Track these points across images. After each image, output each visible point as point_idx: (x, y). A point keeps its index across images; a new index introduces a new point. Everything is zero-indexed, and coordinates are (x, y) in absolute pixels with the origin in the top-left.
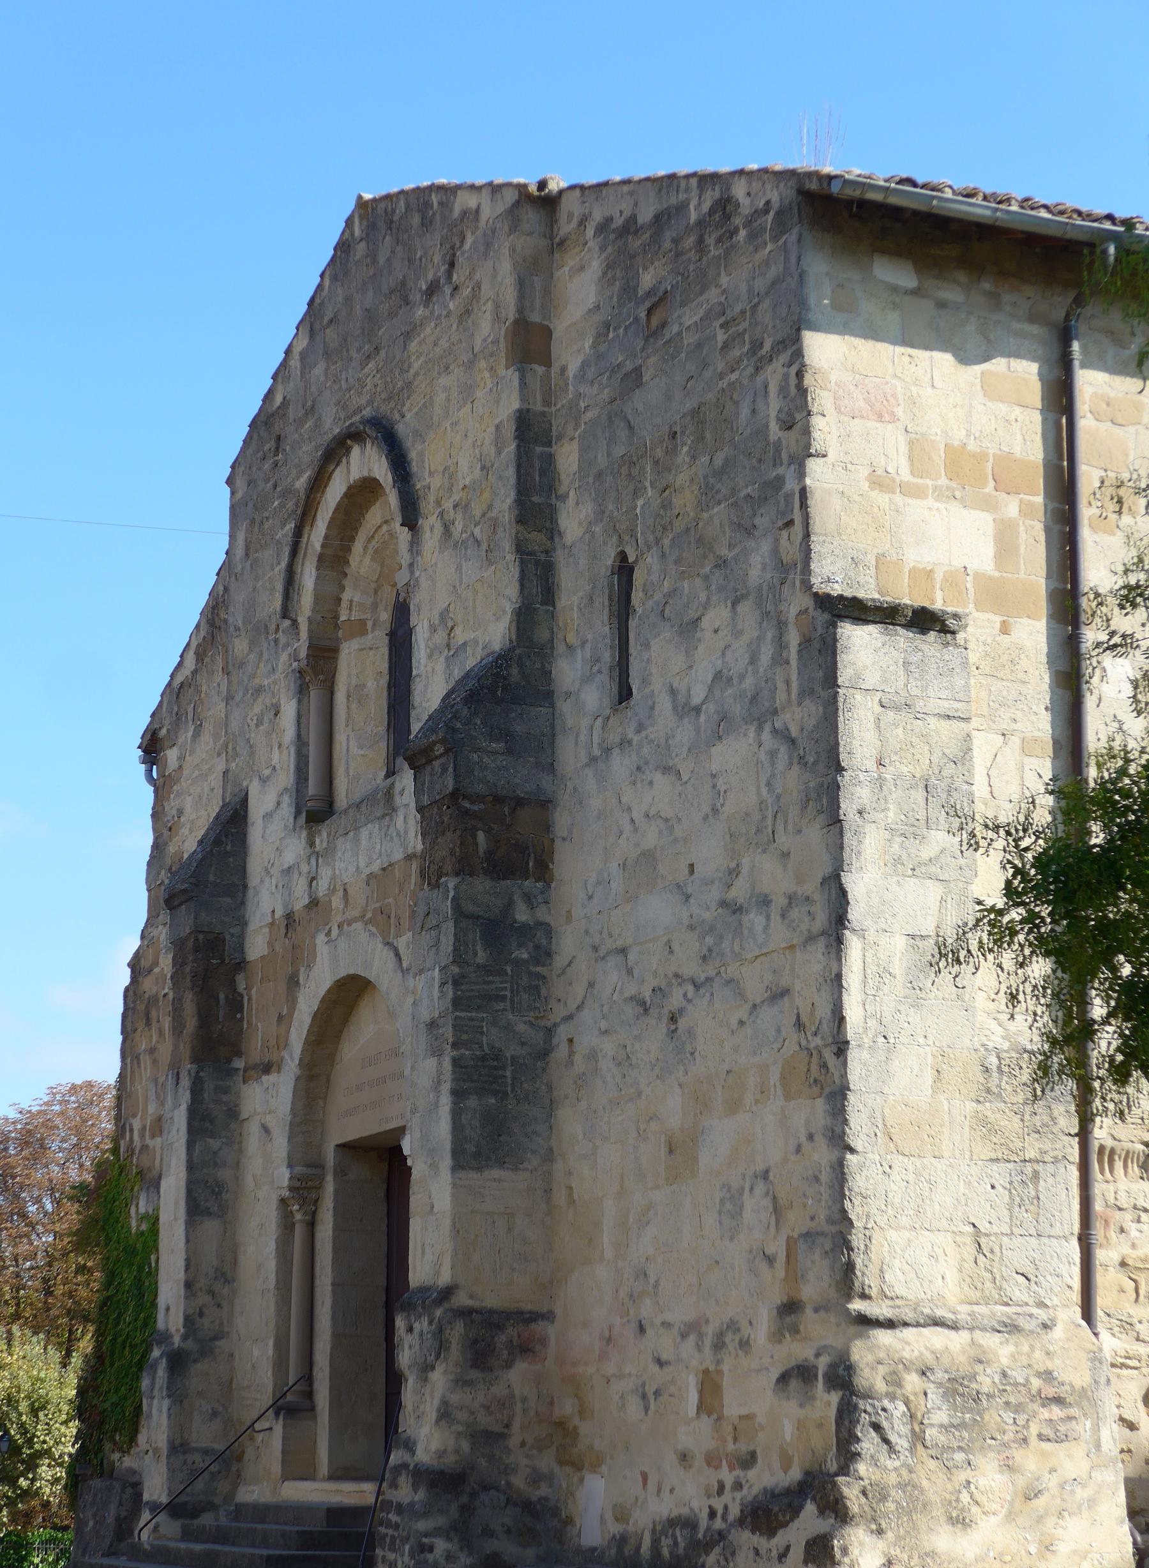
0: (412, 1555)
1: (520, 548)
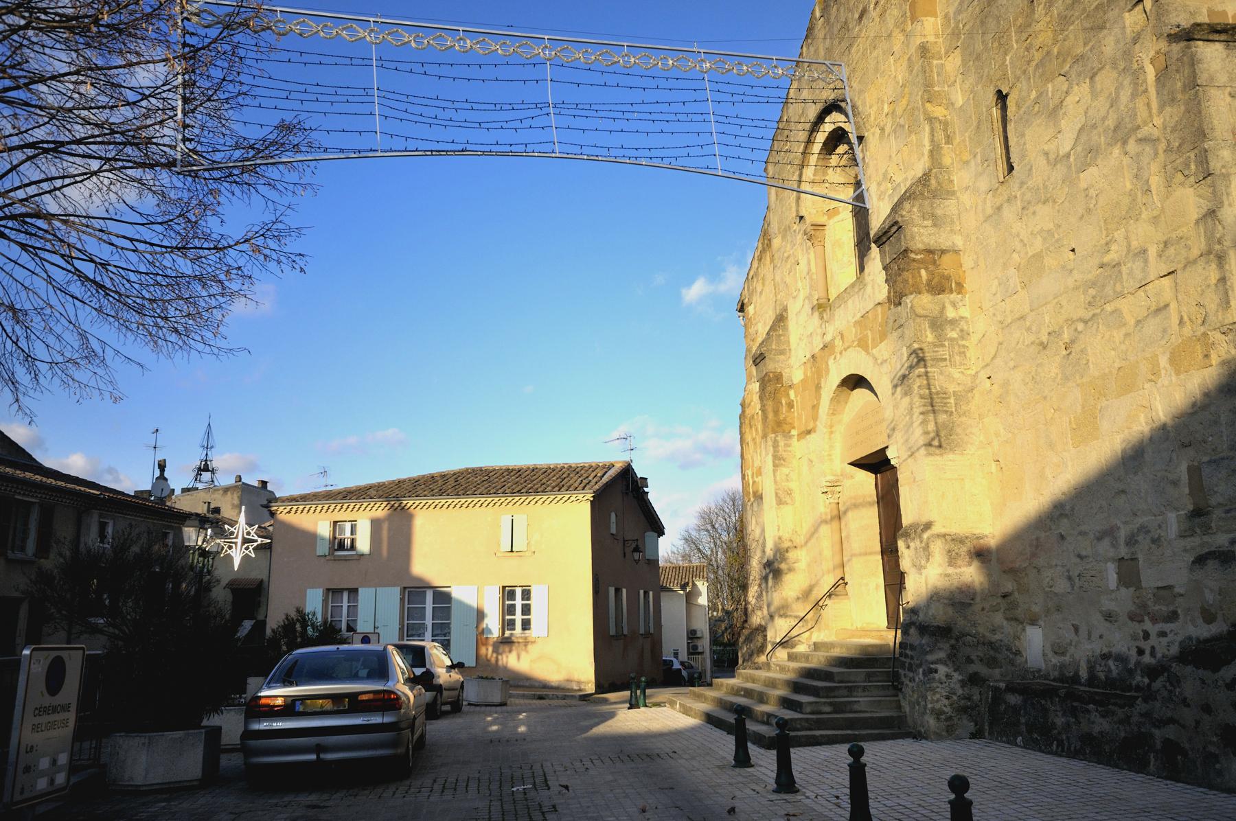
0: (924, 674)
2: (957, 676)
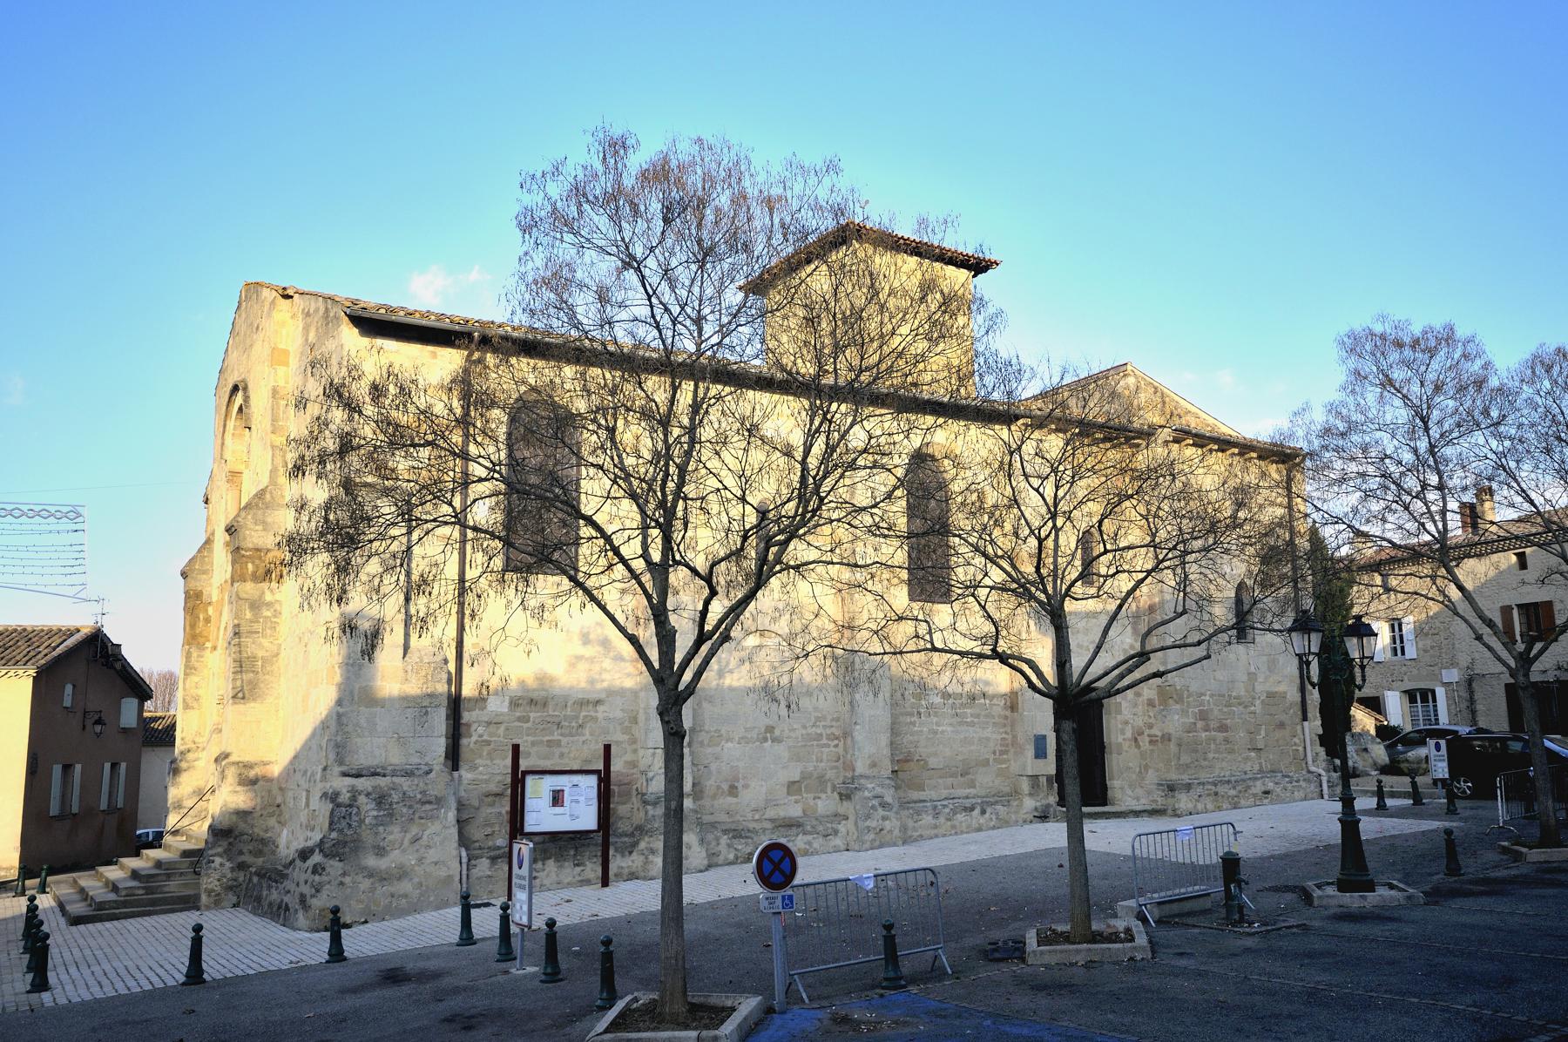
2: (228, 865)
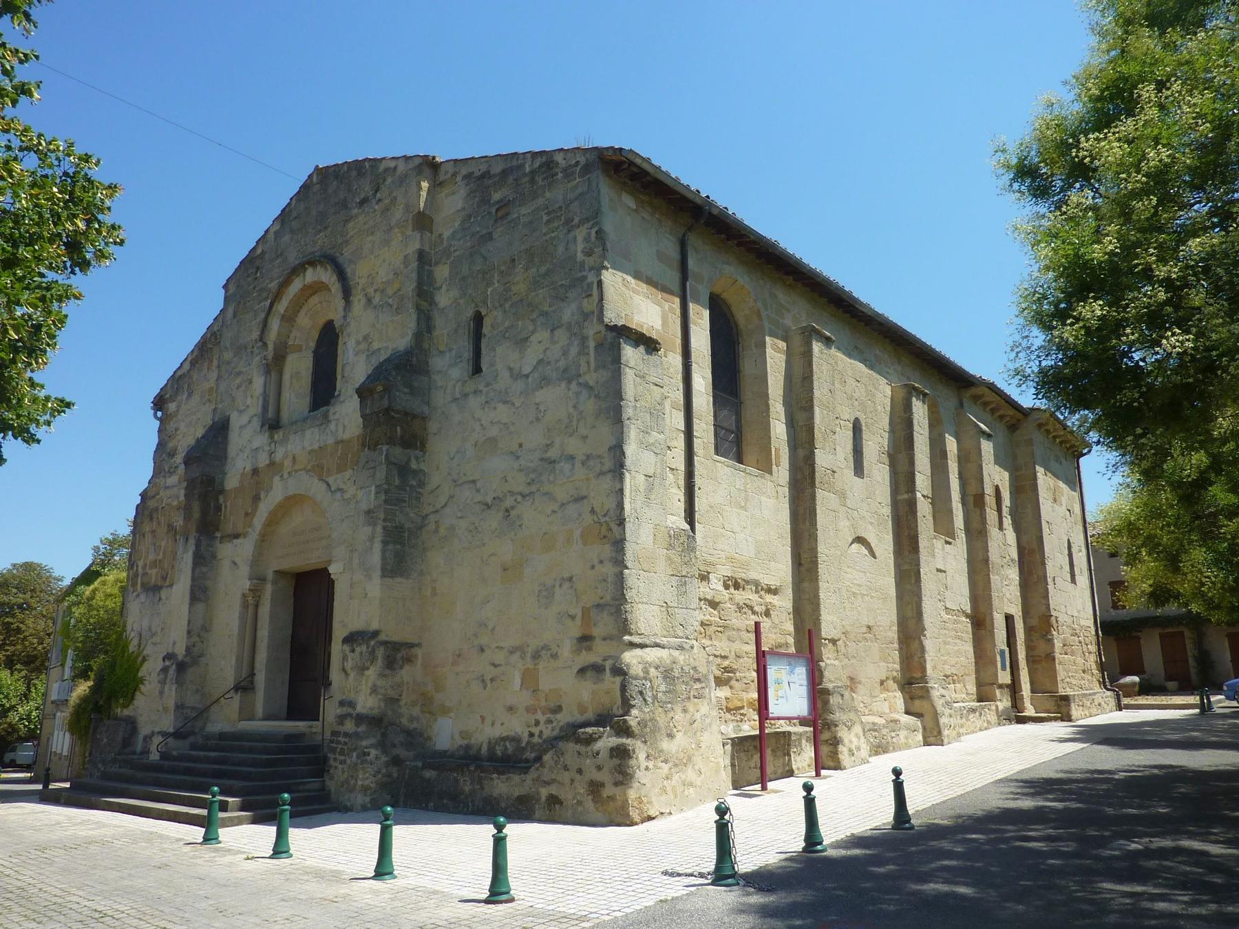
0: (358, 757)
1: (418, 308)
2: (384, 759)
